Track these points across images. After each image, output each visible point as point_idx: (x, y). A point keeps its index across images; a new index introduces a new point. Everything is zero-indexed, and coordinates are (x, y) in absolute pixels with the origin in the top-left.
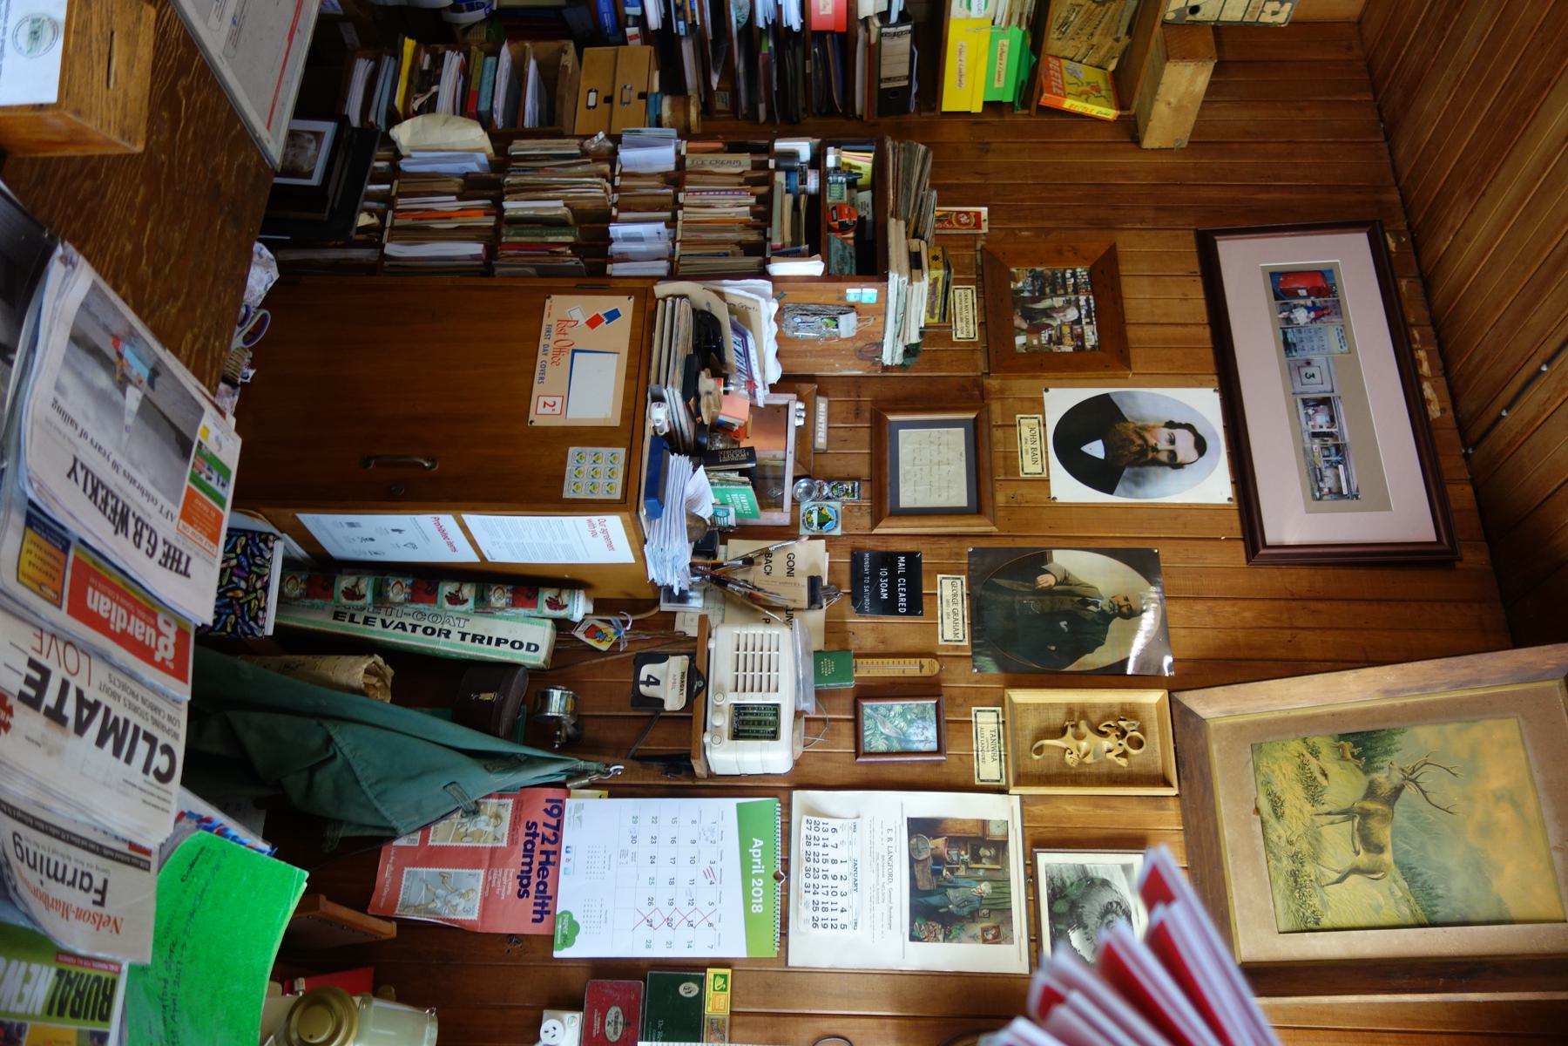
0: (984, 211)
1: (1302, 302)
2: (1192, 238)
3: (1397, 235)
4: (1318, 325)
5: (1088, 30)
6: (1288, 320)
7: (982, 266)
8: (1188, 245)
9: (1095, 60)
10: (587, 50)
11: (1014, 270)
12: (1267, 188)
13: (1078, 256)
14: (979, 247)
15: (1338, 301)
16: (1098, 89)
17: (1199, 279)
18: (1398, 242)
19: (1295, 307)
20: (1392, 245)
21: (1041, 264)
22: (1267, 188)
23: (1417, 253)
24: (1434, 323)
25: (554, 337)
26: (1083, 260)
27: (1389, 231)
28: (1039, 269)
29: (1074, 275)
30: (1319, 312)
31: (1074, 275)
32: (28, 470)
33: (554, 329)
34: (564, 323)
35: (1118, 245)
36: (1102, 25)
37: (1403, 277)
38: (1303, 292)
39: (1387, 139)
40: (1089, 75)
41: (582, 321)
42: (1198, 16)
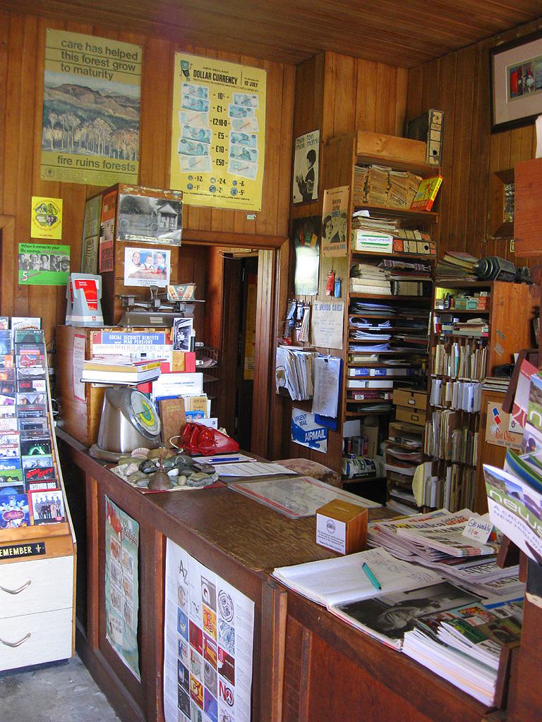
0: (254, 180)
1: (524, 82)
2: (494, 136)
3: (497, 41)
4: (534, 73)
5: (402, 191)
6: (532, 87)
7: (503, 236)
8: (498, 138)
9: (416, 187)
10: (201, 375)
11: (504, 221)
12: (475, 103)
13: (500, 190)
14: (494, 238)
15: (524, 65)
16: (428, 185)
17: (513, 131)
18: (500, 40)
19: (526, 85)
20: (501, 42)
21: (502, 208)
22: (475, 103)
23: (505, 31)
24: (536, 19)
25: (503, 440)
26: (501, 187)
27: (496, 44)
28: (504, 209)
29: (508, 192)
30: (529, 73)
31: (508, 192)
32: (374, 664)
33: (500, 440)
34: (497, 435)
35: (496, 171)
36: (401, 185)
37: (515, 35)
38: (520, 82)
39: (457, 50)
40: (422, 190)
41: (497, 426)
42: (438, 150)
